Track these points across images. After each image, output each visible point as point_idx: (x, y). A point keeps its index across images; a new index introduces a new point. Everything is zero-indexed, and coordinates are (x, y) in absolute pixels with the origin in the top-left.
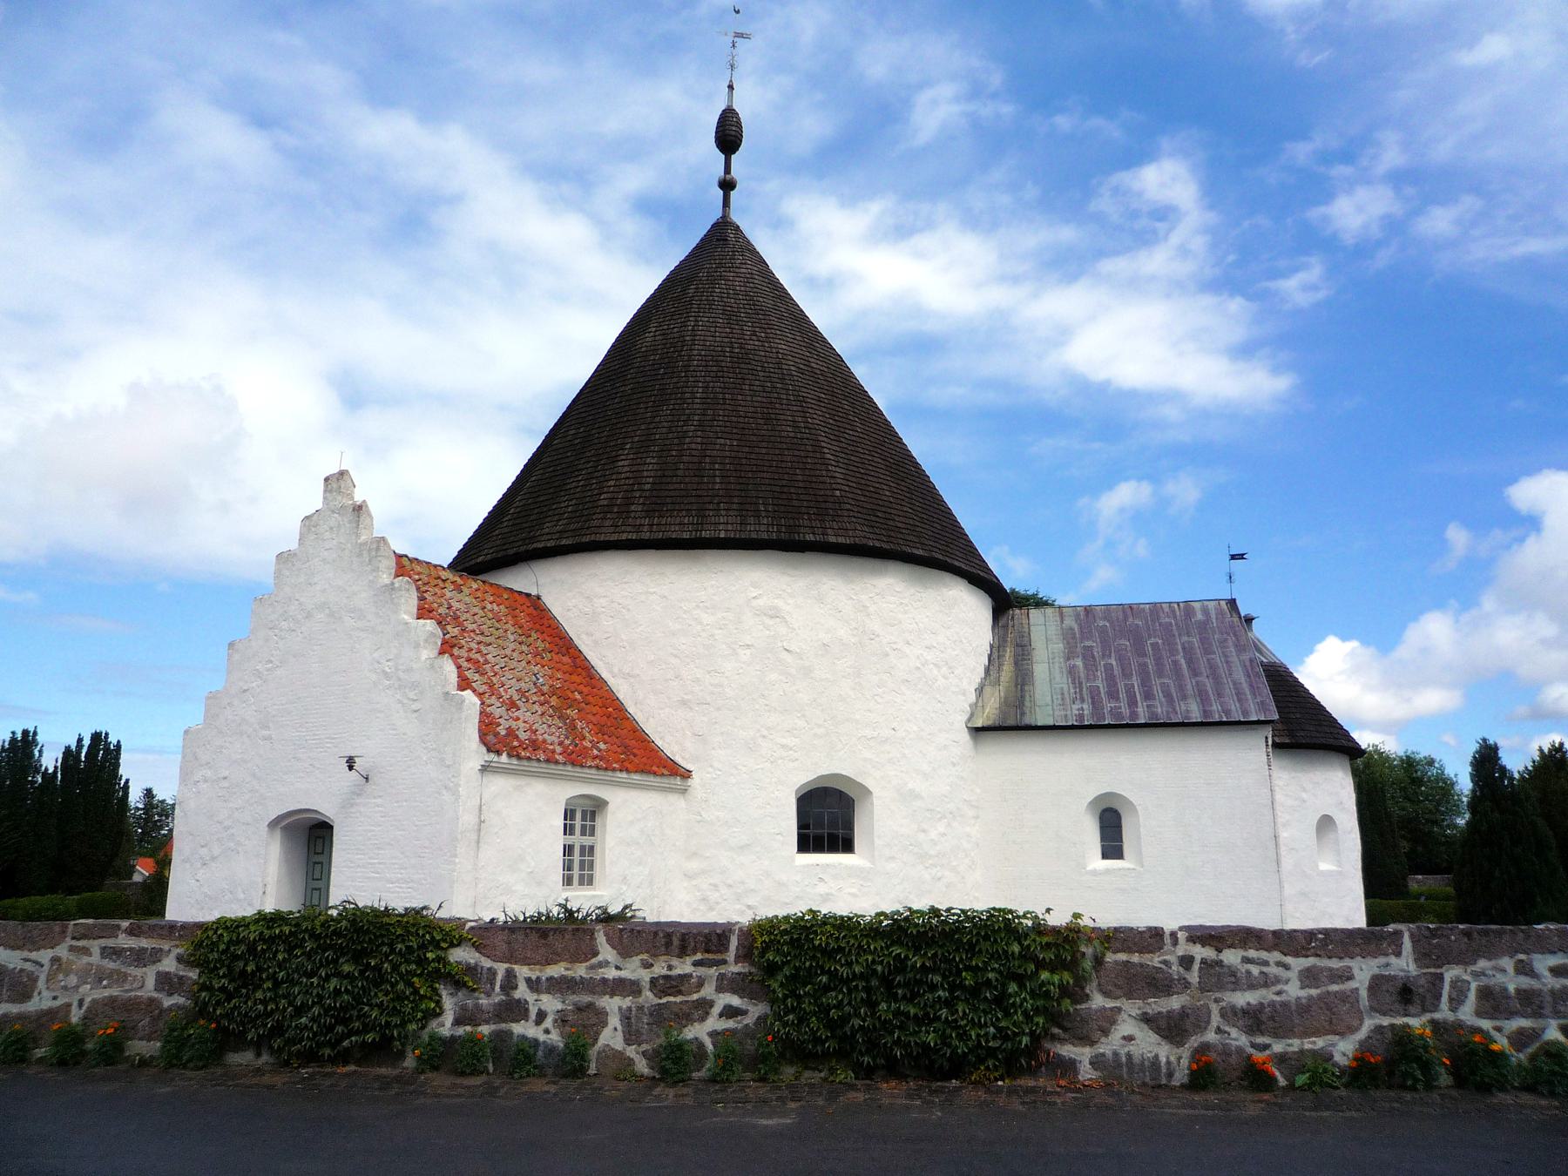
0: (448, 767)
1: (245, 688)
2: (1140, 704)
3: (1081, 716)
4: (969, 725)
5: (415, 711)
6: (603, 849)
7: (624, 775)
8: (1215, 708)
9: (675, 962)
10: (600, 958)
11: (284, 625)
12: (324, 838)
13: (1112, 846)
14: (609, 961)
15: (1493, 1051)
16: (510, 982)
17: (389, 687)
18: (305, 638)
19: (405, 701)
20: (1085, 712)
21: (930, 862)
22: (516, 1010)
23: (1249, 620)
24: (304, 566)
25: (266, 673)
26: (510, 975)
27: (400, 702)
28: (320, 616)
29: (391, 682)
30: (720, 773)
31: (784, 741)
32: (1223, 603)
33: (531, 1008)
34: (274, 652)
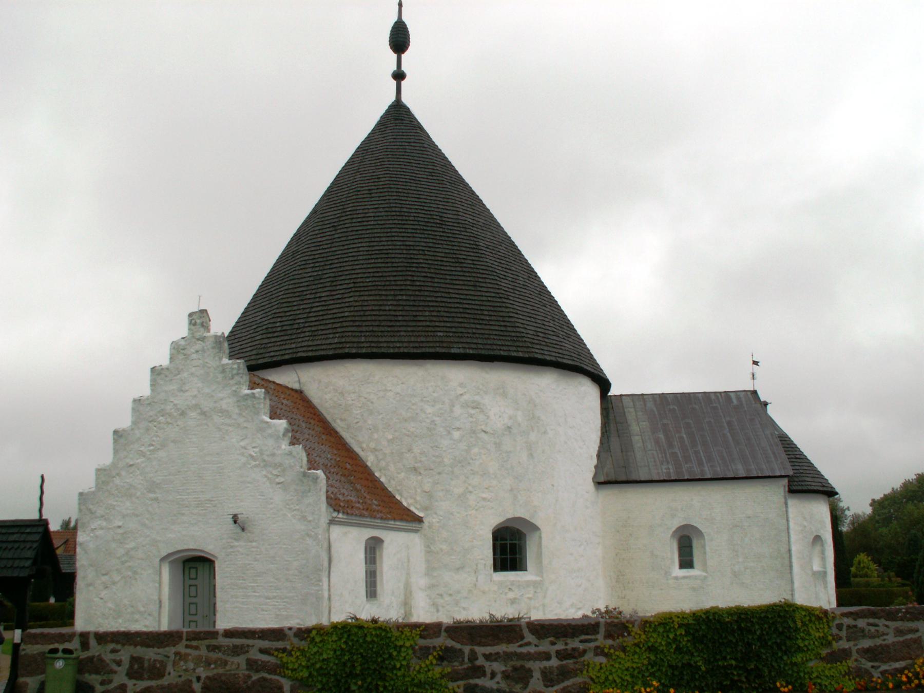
0: (310, 521)
1: (131, 463)
2: (705, 465)
3: (669, 473)
4: (595, 481)
5: (279, 483)
6: (382, 573)
7: (392, 522)
8: (753, 467)
9: (569, 641)
10: (525, 641)
11: (162, 419)
12: (196, 568)
13: (686, 562)
14: (533, 645)
15: (893, 687)
16: (473, 656)
17: (256, 466)
18: (181, 429)
19: (270, 476)
20: (671, 471)
21: (575, 574)
22: (479, 671)
23: (766, 404)
24: (175, 378)
25: (149, 453)
26: (473, 653)
27: (266, 476)
28: (193, 414)
29: (257, 463)
30: (441, 518)
31: (484, 495)
32: (749, 393)
33: (487, 670)
34: (154, 439)
